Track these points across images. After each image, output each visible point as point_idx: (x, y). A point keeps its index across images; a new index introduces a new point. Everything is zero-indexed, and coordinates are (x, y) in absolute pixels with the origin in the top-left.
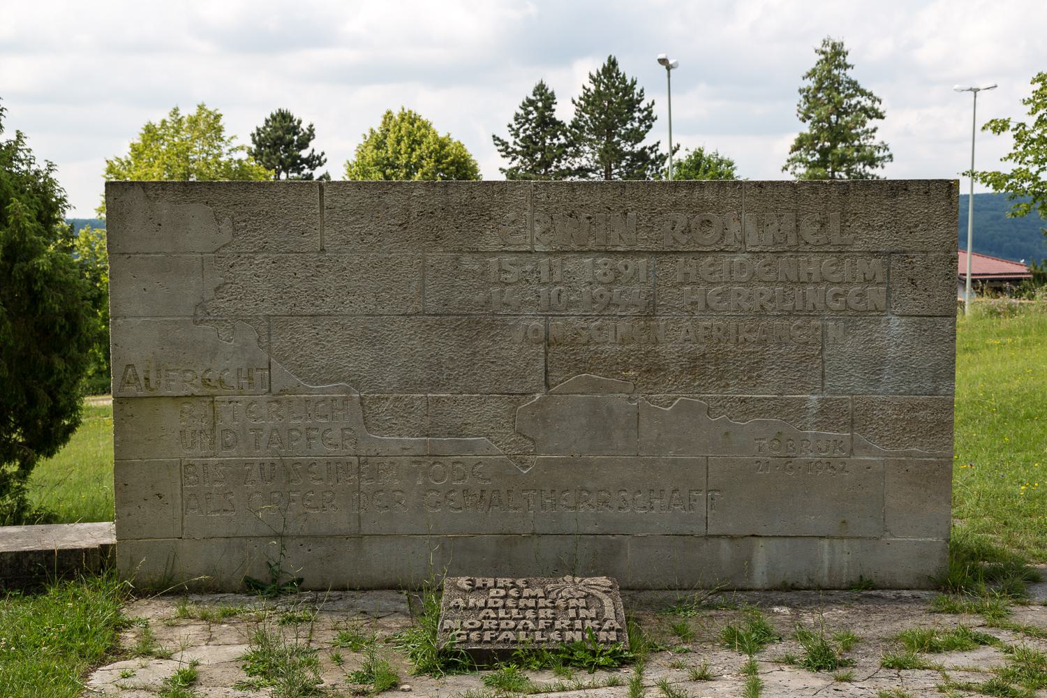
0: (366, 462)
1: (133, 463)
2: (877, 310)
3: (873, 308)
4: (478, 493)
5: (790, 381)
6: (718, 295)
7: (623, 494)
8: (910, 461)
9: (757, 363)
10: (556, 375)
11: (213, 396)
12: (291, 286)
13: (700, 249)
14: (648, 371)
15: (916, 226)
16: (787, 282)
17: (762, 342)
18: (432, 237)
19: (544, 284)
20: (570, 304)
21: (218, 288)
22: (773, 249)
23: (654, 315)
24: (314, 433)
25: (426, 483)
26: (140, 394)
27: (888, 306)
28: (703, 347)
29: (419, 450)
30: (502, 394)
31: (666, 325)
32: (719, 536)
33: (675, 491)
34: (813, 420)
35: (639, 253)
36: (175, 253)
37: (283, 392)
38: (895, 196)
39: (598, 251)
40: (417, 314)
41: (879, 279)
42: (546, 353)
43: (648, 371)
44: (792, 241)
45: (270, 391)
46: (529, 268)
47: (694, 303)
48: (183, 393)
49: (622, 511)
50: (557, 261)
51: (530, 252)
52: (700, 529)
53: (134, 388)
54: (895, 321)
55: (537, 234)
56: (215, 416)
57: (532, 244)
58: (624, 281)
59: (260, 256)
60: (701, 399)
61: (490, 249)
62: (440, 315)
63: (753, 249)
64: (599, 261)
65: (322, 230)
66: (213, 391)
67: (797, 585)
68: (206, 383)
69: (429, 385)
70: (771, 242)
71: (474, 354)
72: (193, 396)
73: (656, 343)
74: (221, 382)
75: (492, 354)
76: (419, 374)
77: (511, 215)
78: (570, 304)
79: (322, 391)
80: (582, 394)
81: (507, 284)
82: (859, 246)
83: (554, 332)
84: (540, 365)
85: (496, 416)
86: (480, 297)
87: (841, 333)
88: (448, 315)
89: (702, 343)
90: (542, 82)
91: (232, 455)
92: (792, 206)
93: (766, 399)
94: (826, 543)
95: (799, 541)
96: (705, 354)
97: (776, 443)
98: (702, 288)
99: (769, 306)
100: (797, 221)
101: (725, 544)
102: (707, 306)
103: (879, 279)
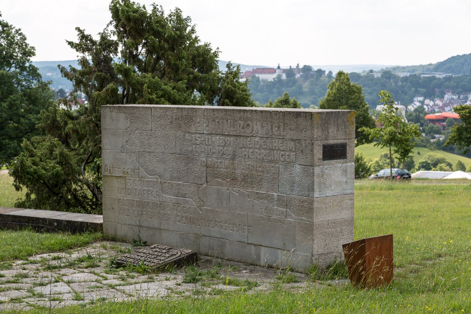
0: (162, 204)
1: (107, 197)
2: (293, 162)
3: (292, 161)
4: (189, 218)
5: (270, 187)
6: (251, 153)
7: (226, 224)
8: (302, 223)
9: (261, 179)
10: (209, 179)
11: (125, 177)
12: (144, 142)
13: (246, 135)
14: (233, 179)
15: (303, 130)
16: (269, 149)
17: (263, 171)
18: (178, 127)
19: (207, 145)
20: (213, 153)
21: (127, 141)
22: (266, 136)
23: (235, 159)
24: (149, 192)
25: (176, 213)
26: (108, 175)
27: (296, 161)
28: (247, 172)
29: (174, 201)
30: (195, 184)
31: (238, 163)
32: (251, 244)
33: (240, 225)
34: (276, 203)
35: (231, 136)
36: (116, 129)
37: (142, 177)
38: (297, 117)
39: (220, 134)
40: (174, 153)
41: (293, 150)
42: (206, 170)
43: (233, 179)
44: (270, 134)
45: (139, 177)
46: (203, 139)
47: (245, 155)
48: (118, 175)
49: (226, 231)
50: (210, 137)
51: (203, 133)
52: (246, 241)
53: (107, 173)
54: (298, 166)
55: (204, 127)
56: (126, 184)
57: (203, 131)
58: (227, 145)
59: (137, 131)
60: (246, 191)
61: (193, 132)
62: (180, 154)
63: (260, 136)
64: (221, 138)
65: (151, 123)
66: (126, 175)
67: (253, 264)
68: (124, 172)
69: (178, 179)
70: (265, 134)
71: (188, 169)
72: (121, 176)
73: (235, 169)
74: (127, 172)
75: (193, 169)
76: (175, 175)
77: (198, 120)
78: (213, 153)
79: (151, 178)
80: (215, 186)
81: (197, 145)
82: (288, 137)
83: (209, 163)
84: (205, 175)
85: (193, 192)
86: (190, 149)
87: (283, 170)
88: (182, 154)
89: (247, 170)
90: (49, 83)
91: (129, 197)
92: (270, 120)
93: (263, 193)
94: (280, 251)
95: (273, 249)
96: (247, 175)
97: (266, 210)
98: (247, 150)
99: (265, 158)
100: (272, 126)
101: (253, 247)
102: (249, 156)
103: (293, 150)
